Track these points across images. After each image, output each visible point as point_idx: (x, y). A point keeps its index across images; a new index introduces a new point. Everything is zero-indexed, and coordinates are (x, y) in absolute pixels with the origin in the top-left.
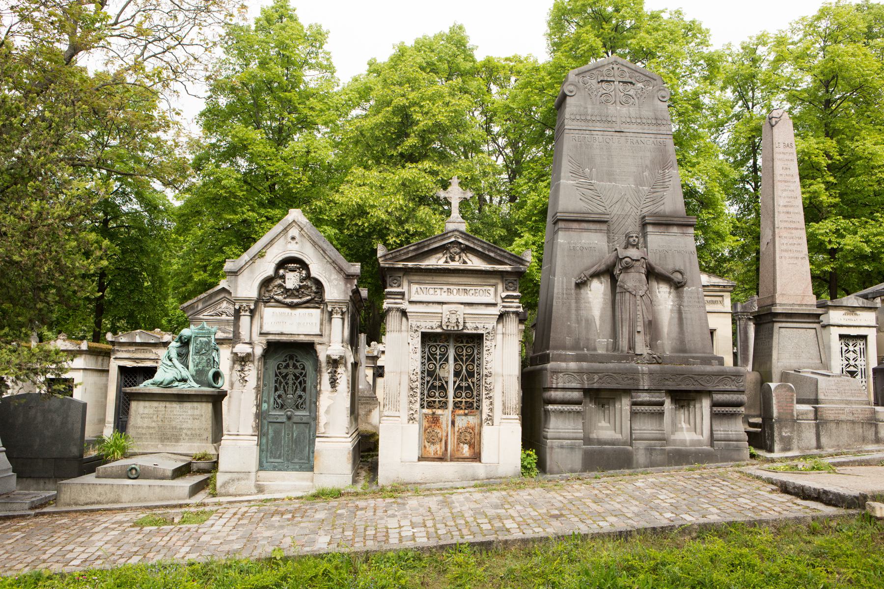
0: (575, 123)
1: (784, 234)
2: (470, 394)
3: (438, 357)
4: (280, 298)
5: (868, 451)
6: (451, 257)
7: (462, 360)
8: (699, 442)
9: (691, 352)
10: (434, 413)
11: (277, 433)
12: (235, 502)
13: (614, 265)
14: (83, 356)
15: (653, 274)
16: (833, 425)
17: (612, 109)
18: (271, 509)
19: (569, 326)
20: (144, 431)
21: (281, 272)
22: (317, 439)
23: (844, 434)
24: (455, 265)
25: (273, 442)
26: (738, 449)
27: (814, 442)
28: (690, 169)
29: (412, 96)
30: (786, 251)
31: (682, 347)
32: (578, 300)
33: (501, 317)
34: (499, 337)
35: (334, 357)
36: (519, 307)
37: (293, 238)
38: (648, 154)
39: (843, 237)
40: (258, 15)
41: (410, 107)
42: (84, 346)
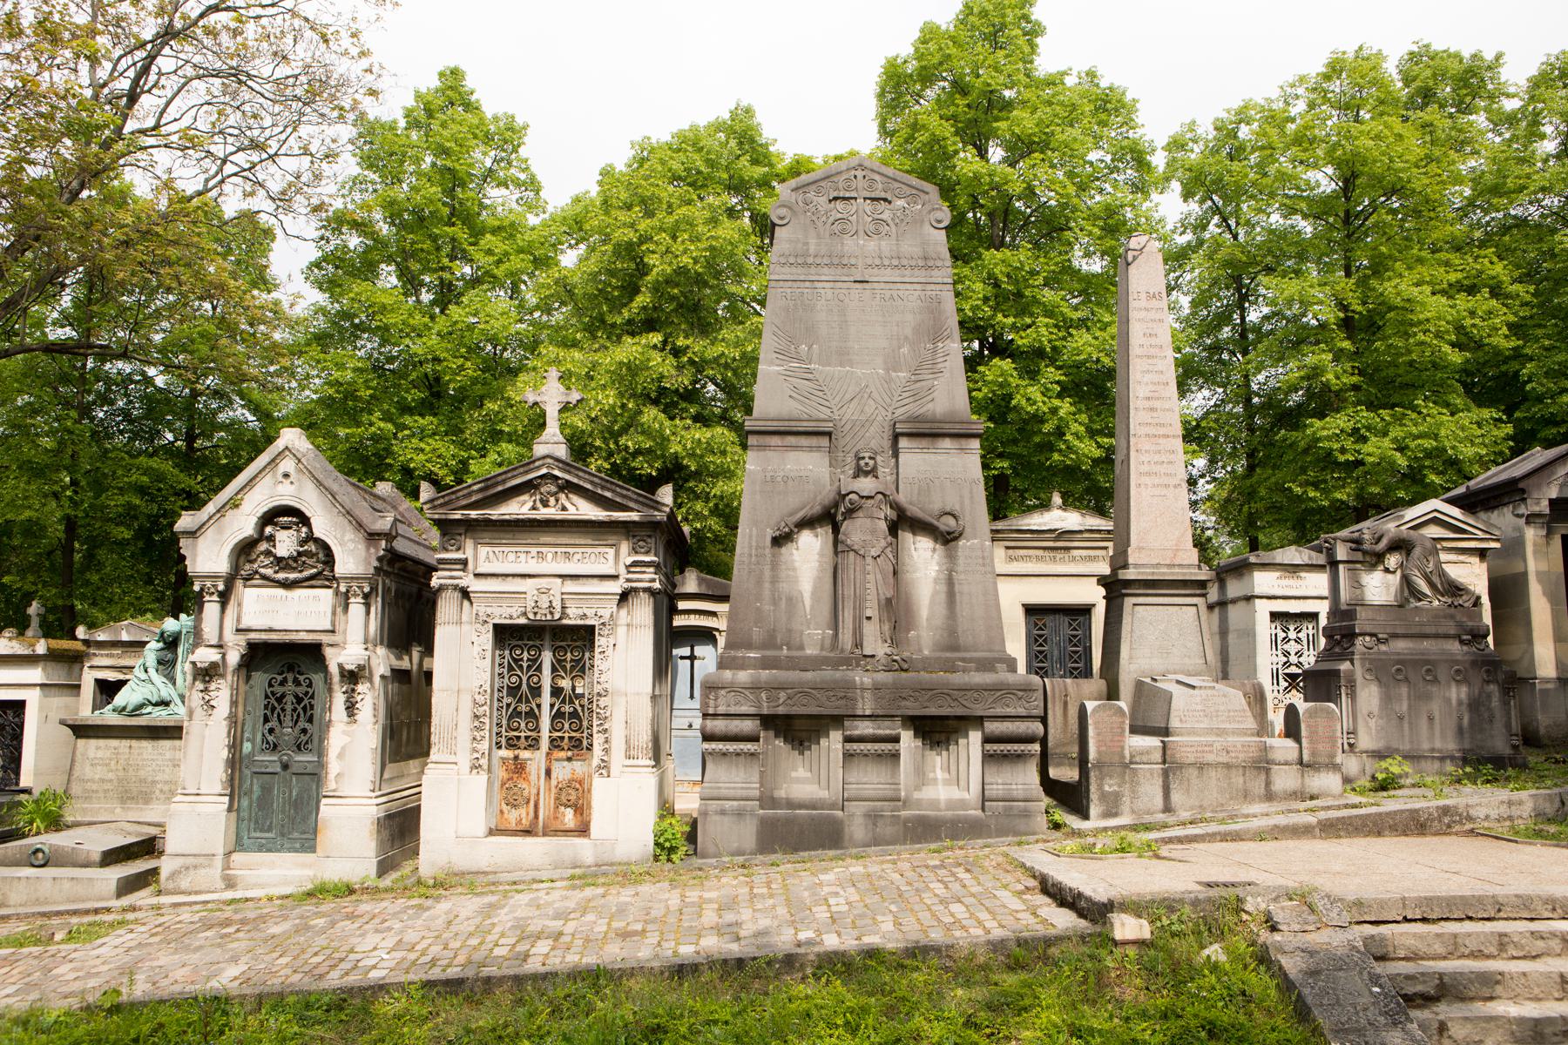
0: (786, 269)
1: (1145, 445)
2: (575, 727)
3: (525, 665)
4: (269, 572)
5: (1247, 816)
6: (542, 501)
7: (564, 668)
8: (962, 804)
9: (966, 650)
10: (516, 758)
11: (266, 790)
12: (184, 904)
13: (836, 505)
14: (41, 664)
15: (903, 522)
16: (1194, 772)
17: (849, 244)
18: (233, 917)
19: (758, 609)
20: (94, 787)
21: (268, 530)
22: (324, 801)
23: (1212, 789)
24: (550, 512)
25: (259, 806)
26: (1026, 814)
27: (1159, 801)
28: (1098, 334)
29: (643, 225)
30: (1148, 474)
31: (952, 642)
32: (775, 566)
33: (624, 597)
34: (621, 631)
35: (348, 667)
36: (653, 580)
37: (286, 476)
38: (909, 317)
39: (1364, 440)
40: (410, 102)
41: (641, 243)
42: (41, 648)
